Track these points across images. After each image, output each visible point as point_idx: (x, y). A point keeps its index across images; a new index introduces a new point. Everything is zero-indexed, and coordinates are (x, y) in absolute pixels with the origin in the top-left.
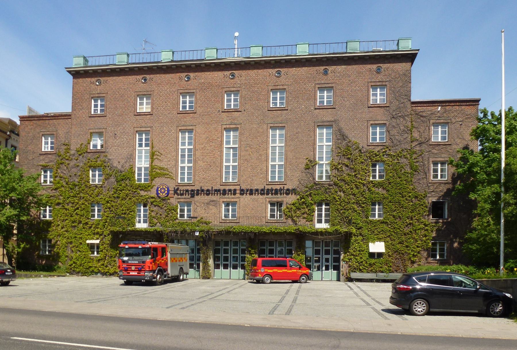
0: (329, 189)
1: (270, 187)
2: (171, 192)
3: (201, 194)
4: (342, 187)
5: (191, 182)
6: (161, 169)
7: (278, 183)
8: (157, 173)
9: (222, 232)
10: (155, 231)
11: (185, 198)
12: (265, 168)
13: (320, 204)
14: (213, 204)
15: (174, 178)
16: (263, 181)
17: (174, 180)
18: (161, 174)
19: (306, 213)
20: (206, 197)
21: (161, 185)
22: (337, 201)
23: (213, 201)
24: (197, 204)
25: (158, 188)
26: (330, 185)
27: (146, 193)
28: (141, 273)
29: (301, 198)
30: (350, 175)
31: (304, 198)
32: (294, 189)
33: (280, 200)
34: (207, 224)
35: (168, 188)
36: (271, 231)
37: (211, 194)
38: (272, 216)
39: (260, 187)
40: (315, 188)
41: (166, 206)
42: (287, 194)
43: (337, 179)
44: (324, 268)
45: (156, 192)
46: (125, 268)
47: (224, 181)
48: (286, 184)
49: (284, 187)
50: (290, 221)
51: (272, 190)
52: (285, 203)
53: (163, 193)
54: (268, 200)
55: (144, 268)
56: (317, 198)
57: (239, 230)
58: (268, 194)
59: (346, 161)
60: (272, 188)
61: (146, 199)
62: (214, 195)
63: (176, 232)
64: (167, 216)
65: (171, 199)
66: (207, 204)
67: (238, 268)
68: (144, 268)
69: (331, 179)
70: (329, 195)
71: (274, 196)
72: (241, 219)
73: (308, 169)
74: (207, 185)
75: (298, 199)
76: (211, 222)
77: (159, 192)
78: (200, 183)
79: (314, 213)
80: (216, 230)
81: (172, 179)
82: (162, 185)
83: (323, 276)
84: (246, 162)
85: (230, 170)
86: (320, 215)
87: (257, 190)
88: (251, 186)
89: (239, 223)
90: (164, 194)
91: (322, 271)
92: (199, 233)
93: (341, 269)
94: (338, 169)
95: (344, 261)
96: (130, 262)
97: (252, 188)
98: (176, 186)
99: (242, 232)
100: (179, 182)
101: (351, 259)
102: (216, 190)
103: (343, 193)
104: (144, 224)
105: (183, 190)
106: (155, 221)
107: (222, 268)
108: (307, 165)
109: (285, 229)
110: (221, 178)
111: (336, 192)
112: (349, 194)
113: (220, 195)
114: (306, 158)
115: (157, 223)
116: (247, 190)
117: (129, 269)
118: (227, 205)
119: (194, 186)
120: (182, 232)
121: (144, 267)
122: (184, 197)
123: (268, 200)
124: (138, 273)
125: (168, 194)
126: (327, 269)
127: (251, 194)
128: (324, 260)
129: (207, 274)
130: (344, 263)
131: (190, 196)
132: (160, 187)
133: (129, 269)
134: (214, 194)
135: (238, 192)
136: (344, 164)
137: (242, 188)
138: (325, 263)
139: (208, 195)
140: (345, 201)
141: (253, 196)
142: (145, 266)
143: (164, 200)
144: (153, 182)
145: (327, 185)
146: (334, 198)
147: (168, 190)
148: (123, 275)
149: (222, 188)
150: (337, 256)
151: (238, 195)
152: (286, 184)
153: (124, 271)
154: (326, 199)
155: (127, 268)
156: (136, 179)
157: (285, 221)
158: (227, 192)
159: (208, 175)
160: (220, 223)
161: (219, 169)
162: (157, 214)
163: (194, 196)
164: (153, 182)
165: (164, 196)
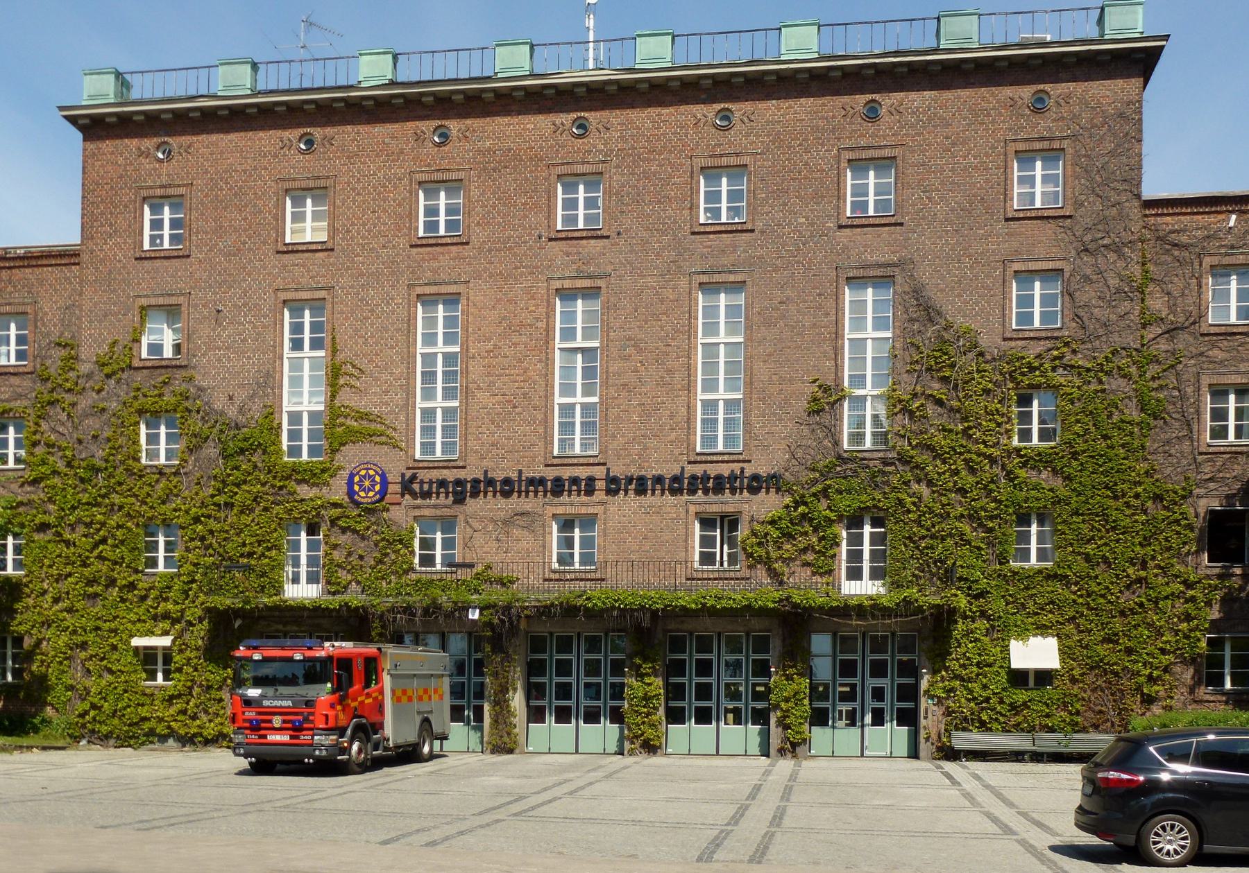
0: (884, 473)
1: (698, 470)
2: (391, 488)
5: (455, 457)
6: (362, 418)
8: (349, 430)
11: (435, 506)
12: (684, 411)
13: (855, 522)
14: (521, 523)
15: (403, 445)
16: (676, 452)
17: (401, 450)
18: (361, 433)
20: (502, 502)
21: (374, 467)
22: (909, 511)
25: (352, 476)
26: (886, 462)
27: (313, 492)
28: (302, 737)
29: (797, 504)
30: (950, 431)
31: (805, 504)
33: (729, 508)
34: (503, 585)
36: (704, 605)
37: (516, 494)
39: (669, 470)
40: (838, 473)
41: (376, 532)
42: (754, 491)
43: (910, 444)
44: (868, 719)
45: (345, 488)
46: (250, 721)
48: (749, 461)
50: (761, 573)
51: (706, 478)
53: (367, 490)
55: (312, 721)
56: (847, 503)
57: (604, 603)
58: (692, 491)
60: (705, 471)
61: (316, 509)
62: (527, 496)
63: (408, 610)
64: (381, 562)
65: (392, 508)
66: (506, 522)
68: (312, 721)
71: (712, 497)
72: (609, 570)
73: (818, 412)
74: (503, 464)
75: (787, 507)
76: (518, 579)
77: (356, 488)
78: (482, 458)
79: (836, 550)
80: (533, 604)
81: (394, 447)
82: (365, 466)
83: (866, 743)
86: (855, 556)
87: (659, 480)
88: (640, 467)
89: (603, 580)
90: (371, 494)
91: (863, 726)
92: (481, 614)
93: (923, 722)
94: (911, 413)
96: (266, 703)
97: (643, 473)
98: (408, 468)
99: (613, 608)
102: (531, 481)
103: (928, 486)
104: (310, 586)
105: (431, 482)
106: (344, 576)
107: (550, 719)
108: (815, 400)
111: (907, 483)
113: (545, 496)
116: (630, 480)
117: (263, 725)
118: (567, 525)
119: (464, 467)
120: (426, 611)
121: (311, 718)
122: (433, 501)
123: (692, 509)
124: (292, 737)
125: (383, 493)
126: (878, 720)
127: (641, 491)
130: (930, 702)
131: (451, 498)
132: (358, 473)
133: (263, 725)
134: (527, 492)
135: (600, 484)
136: (931, 395)
137: (611, 474)
138: (870, 703)
139: (507, 494)
140: (933, 512)
141: (648, 499)
143: (370, 511)
144: (338, 457)
146: (900, 502)
147: (385, 483)
149: (551, 474)
151: (599, 496)
152: (749, 461)
153: (247, 732)
154: (875, 506)
155: (257, 721)
156: (285, 448)
157: (746, 573)
158: (566, 488)
160: (545, 580)
161: (540, 416)
162: (350, 554)
163: (465, 499)
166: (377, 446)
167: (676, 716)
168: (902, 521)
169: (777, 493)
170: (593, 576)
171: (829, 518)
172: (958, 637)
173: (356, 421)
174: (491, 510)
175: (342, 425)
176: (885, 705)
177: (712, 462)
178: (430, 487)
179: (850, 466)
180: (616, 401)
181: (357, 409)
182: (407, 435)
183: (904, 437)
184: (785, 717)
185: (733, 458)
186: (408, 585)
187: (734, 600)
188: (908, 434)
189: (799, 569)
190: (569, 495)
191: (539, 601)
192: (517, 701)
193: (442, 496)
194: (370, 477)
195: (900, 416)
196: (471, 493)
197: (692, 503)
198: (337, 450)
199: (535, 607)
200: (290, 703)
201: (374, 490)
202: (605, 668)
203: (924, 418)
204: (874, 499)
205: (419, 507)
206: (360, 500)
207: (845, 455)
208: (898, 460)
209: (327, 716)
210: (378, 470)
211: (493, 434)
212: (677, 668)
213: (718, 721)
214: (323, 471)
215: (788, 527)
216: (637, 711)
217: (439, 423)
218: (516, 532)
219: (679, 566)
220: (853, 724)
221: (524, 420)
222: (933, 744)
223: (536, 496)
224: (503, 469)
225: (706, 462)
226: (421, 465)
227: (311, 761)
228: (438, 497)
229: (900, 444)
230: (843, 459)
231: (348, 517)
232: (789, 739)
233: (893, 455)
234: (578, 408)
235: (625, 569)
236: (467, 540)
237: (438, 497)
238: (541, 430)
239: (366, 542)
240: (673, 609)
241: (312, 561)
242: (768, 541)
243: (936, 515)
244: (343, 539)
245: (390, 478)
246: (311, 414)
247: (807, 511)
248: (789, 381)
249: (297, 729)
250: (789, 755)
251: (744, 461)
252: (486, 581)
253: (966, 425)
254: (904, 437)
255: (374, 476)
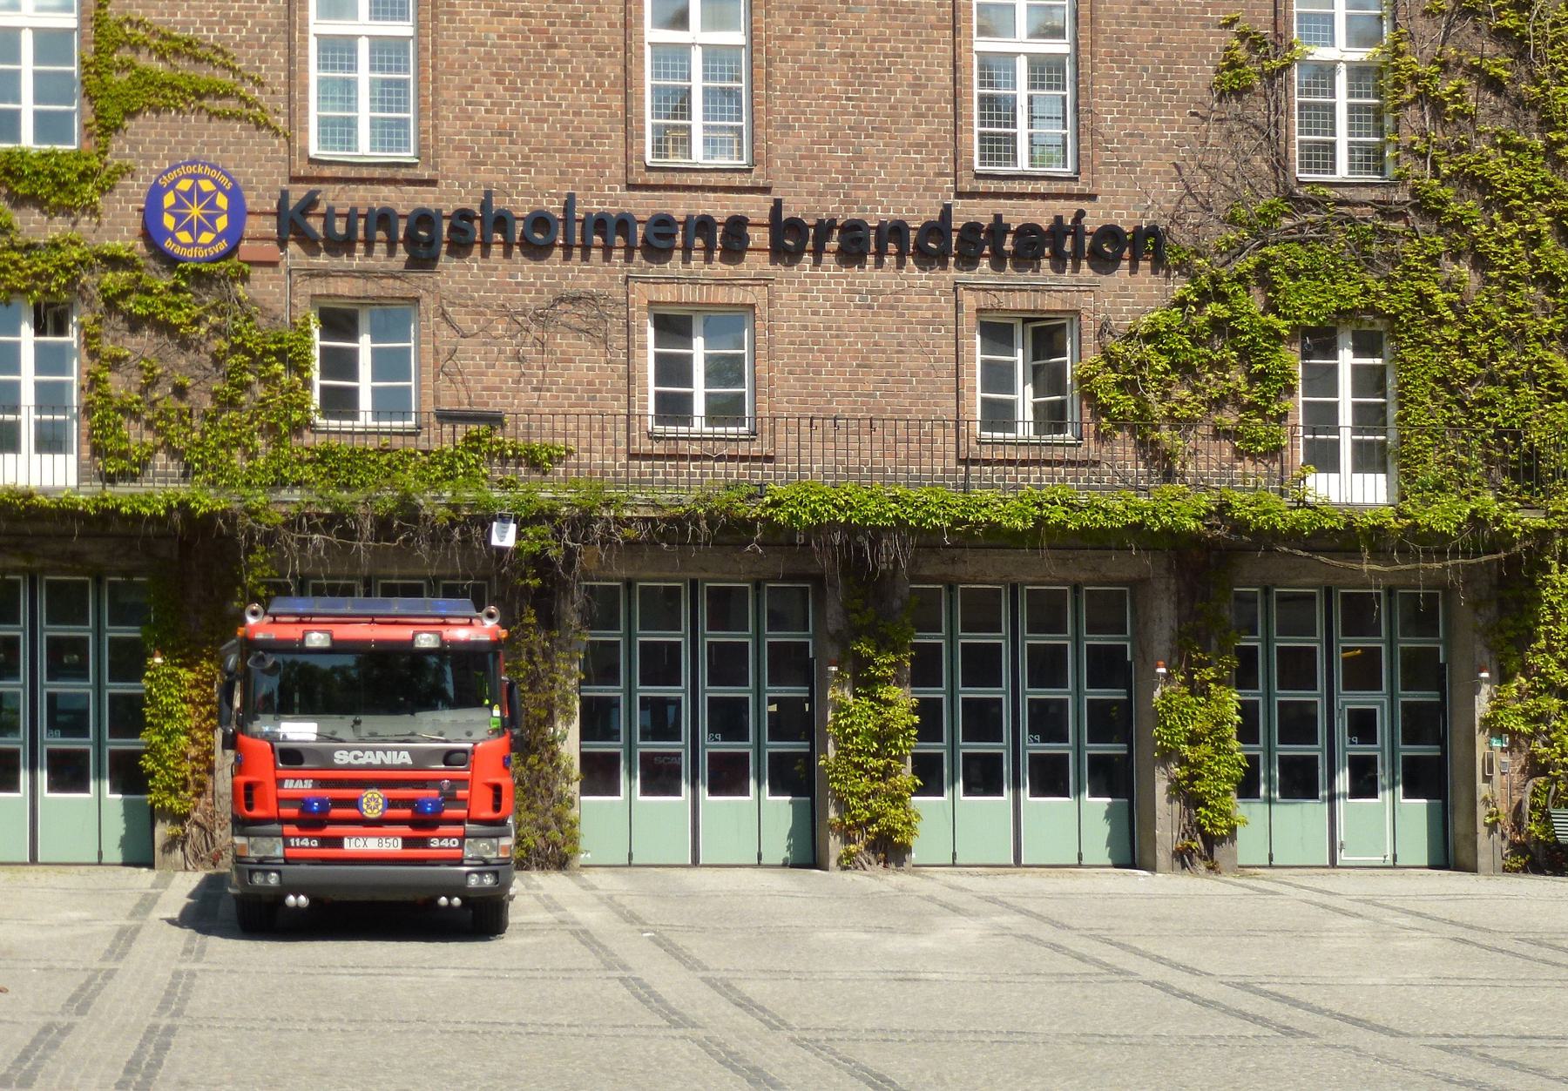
0: (1383, 234)
1: (981, 212)
2: (253, 226)
3: (486, 247)
4: (1465, 229)
5: (408, 156)
6: (176, 52)
7: (1042, 187)
8: (145, 80)
9: (684, 532)
10: (177, 517)
11: (365, 274)
12: (945, 76)
13: (1320, 341)
14: (574, 321)
15: (281, 122)
16: (930, 168)
17: (277, 134)
18: (174, 88)
19: (1237, 402)
20: (525, 269)
21: (182, 171)
22: (1441, 322)
23: (575, 300)
24: (456, 318)
25: (156, 193)
26: (1386, 210)
27: (58, 228)
28: (435, 843)
29: (1204, 297)
30: (1520, 148)
31: (1222, 297)
32: (1153, 231)
33: (1052, 302)
34: (535, 465)
35: (235, 196)
36: (1040, 521)
37: (558, 252)
38: (998, 415)
39: (919, 211)
40: (1287, 231)
41: (217, 330)
42: (1104, 264)
43: (1436, 173)
44: (1343, 781)
45: (135, 222)
46: (303, 803)
47: (649, 159)
48: (1092, 197)
49: (1080, 214)
50: (1124, 449)
51: (998, 228)
52: (1090, 326)
53: (195, 228)
54: (970, 300)
55: (462, 802)
56: (1308, 301)
57: (813, 513)
58: (968, 261)
59: (1489, 48)
60: (998, 217)
61: (67, 270)
62: (585, 257)
63: (337, 522)
64: (232, 403)
65: (256, 273)
66: (541, 318)
67: (752, 784)
68: (462, 802)
69: (1391, 171)
70: (1390, 279)
71: (1011, 275)
72: (781, 436)
73: (1238, 93)
74: (526, 179)
75: (1182, 303)
76: (570, 452)
77: (169, 221)
78: (476, 163)
79: (1288, 403)
80: (643, 512)
81: (258, 127)
82: (191, 170)
83: (1341, 836)
84: (807, 29)
85: (1333, 95)
86: (1323, 417)
87: (896, 231)
88: (848, 201)
89: (769, 459)
90: (206, 238)
91: (1332, 798)
92: (520, 535)
93: (1483, 789)
94: (1438, 106)
95: (1499, 732)
96: (341, 758)
97: (855, 215)
98: (295, 179)
99: (834, 524)
100: (314, 150)
101: (1542, 718)
102: (600, 224)
103: (1474, 267)
104: (1358, 476)
105: (352, 217)
106: (135, 436)
107: (630, 784)
108: (1233, 65)
109: (1141, 511)
110: (629, 124)
111: (1433, 260)
112: (1515, 277)
113: (629, 258)
114: (1222, 18)
115: (156, 449)
116: (825, 229)
117: (336, 812)
118: (673, 326)
119: (432, 182)
120: (383, 526)
121: (461, 793)
122: (358, 260)
123: (970, 300)
124: (408, 842)
125: (234, 236)
126: (1364, 786)
127: (852, 253)
128: (1342, 726)
129: (554, 834)
130: (1496, 744)
131: (402, 254)
132: (172, 185)
133: (336, 812)
134: (586, 249)
135: (759, 237)
136: (1477, 69)
137: (785, 215)
138: (1347, 748)
139: (536, 251)
140: (1493, 324)
141: (869, 275)
142: (463, 782)
143: (200, 279)
144: (116, 144)
145: (1368, 212)
146: (1423, 299)
147: (238, 212)
148: (287, 861)
149: (643, 206)
150: (1116, 694)
151: (756, 263)
152: (1092, 197)
153: (291, 829)
154: (1370, 309)
155: (322, 802)
156: (1377, 139)
157: (1090, 449)
158: (679, 240)
159: (533, 106)
160: (632, 456)
161: (613, 71)
162: (152, 383)
163: (436, 258)
164: (113, 147)
165: (203, 253)
166: (215, 123)
167: (930, 777)
168: (1428, 342)
169: (1155, 271)
170: (743, 448)
171: (1277, 332)
172: (1555, 600)
173: (162, 58)
174: (500, 287)
175: (126, 67)
176: (1379, 750)
177: (1009, 196)
178: (351, 228)
179: (1312, 218)
180: (790, 46)
181: (165, 30)
182: (290, 100)
183: (1424, 156)
184: (1193, 778)
185: (391, 176)
186: (301, 461)
187: (1106, 511)
188: (1433, 151)
189: (1202, 444)
190: (686, 259)
191: (655, 506)
192: (570, 744)
193: (380, 249)
194: (202, 196)
195: (1413, 112)
196: (451, 243)
197: (970, 288)
198: (117, 128)
199: (646, 520)
200: (405, 758)
201: (213, 229)
202: (98, 659)
203: (1464, 117)
204: (1366, 292)
205: (325, 274)
206: (178, 251)
207: (1301, 192)
208: (1416, 207)
209: (497, 788)
210: (224, 180)
211: (501, 106)
212: (925, 670)
213: (1016, 785)
214: (84, 177)
215: (1185, 349)
216: (858, 766)
217: (364, 75)
218: (562, 342)
219: (939, 431)
220: (1310, 792)
221: (575, 77)
222: (1503, 836)
223: (607, 256)
224: (527, 192)
225: (997, 195)
226: (327, 172)
227: (303, 900)
228: (369, 251)
229: (1416, 171)
230: (1298, 200)
231: (148, 292)
232: (1201, 828)
233: (1401, 195)
234: (697, 56)
235: (817, 435)
236: (443, 356)
237: (369, 251)
238: (617, 102)
239: (191, 355)
240: (969, 532)
241: (49, 397)
242: (1144, 379)
243: (1499, 332)
244: (142, 344)
245: (250, 202)
246: (43, 36)
247: (1227, 314)
248: (1175, 19)
249: (423, 822)
250: (1202, 867)
251: (1081, 197)
252: (491, 454)
253: (1554, 137)
254: (1424, 156)
255: (213, 195)
